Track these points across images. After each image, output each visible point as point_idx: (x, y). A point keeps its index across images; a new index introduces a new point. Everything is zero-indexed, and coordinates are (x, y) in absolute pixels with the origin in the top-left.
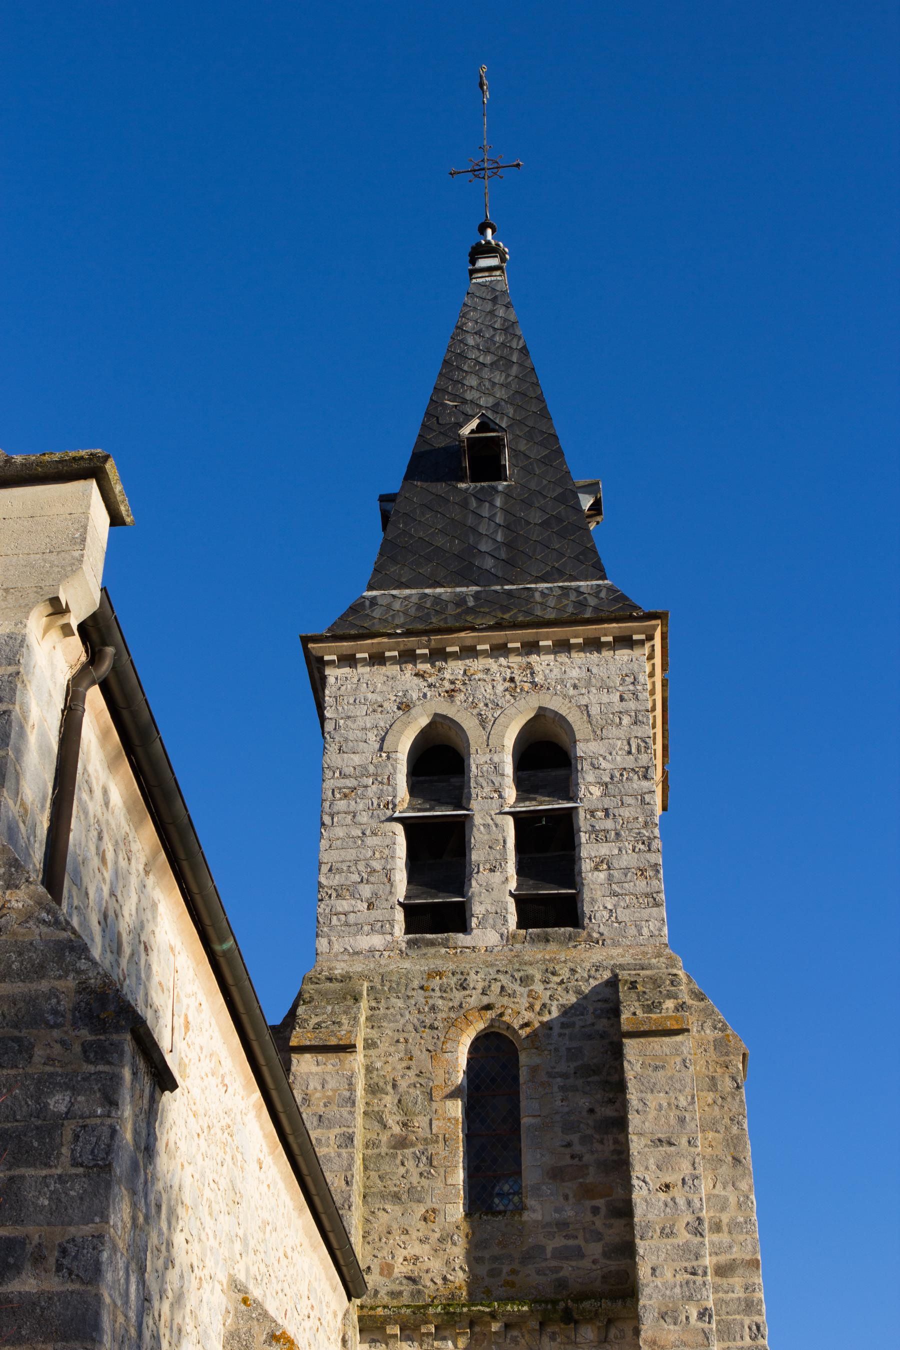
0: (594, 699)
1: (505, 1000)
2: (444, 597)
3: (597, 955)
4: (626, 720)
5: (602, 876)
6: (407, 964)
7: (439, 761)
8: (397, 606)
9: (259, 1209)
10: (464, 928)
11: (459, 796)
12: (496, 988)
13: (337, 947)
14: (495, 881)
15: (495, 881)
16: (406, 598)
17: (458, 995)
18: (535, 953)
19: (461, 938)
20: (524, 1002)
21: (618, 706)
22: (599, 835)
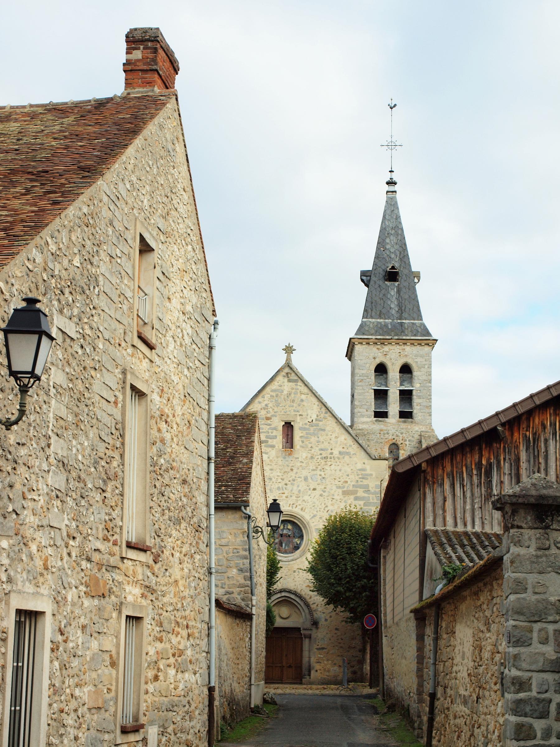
0: (419, 360)
1: (397, 438)
2: (383, 323)
3: (416, 428)
4: (426, 367)
5: (418, 407)
6: (375, 426)
7: (381, 369)
8: (371, 326)
9: (147, 219)
10: (387, 417)
11: (469, 560)
12: (395, 434)
13: (359, 421)
14: (394, 406)
15: (394, 406)
16: (373, 323)
17: (387, 435)
18: (403, 425)
19: (386, 419)
20: (401, 438)
21: (424, 363)
22: (419, 397)
